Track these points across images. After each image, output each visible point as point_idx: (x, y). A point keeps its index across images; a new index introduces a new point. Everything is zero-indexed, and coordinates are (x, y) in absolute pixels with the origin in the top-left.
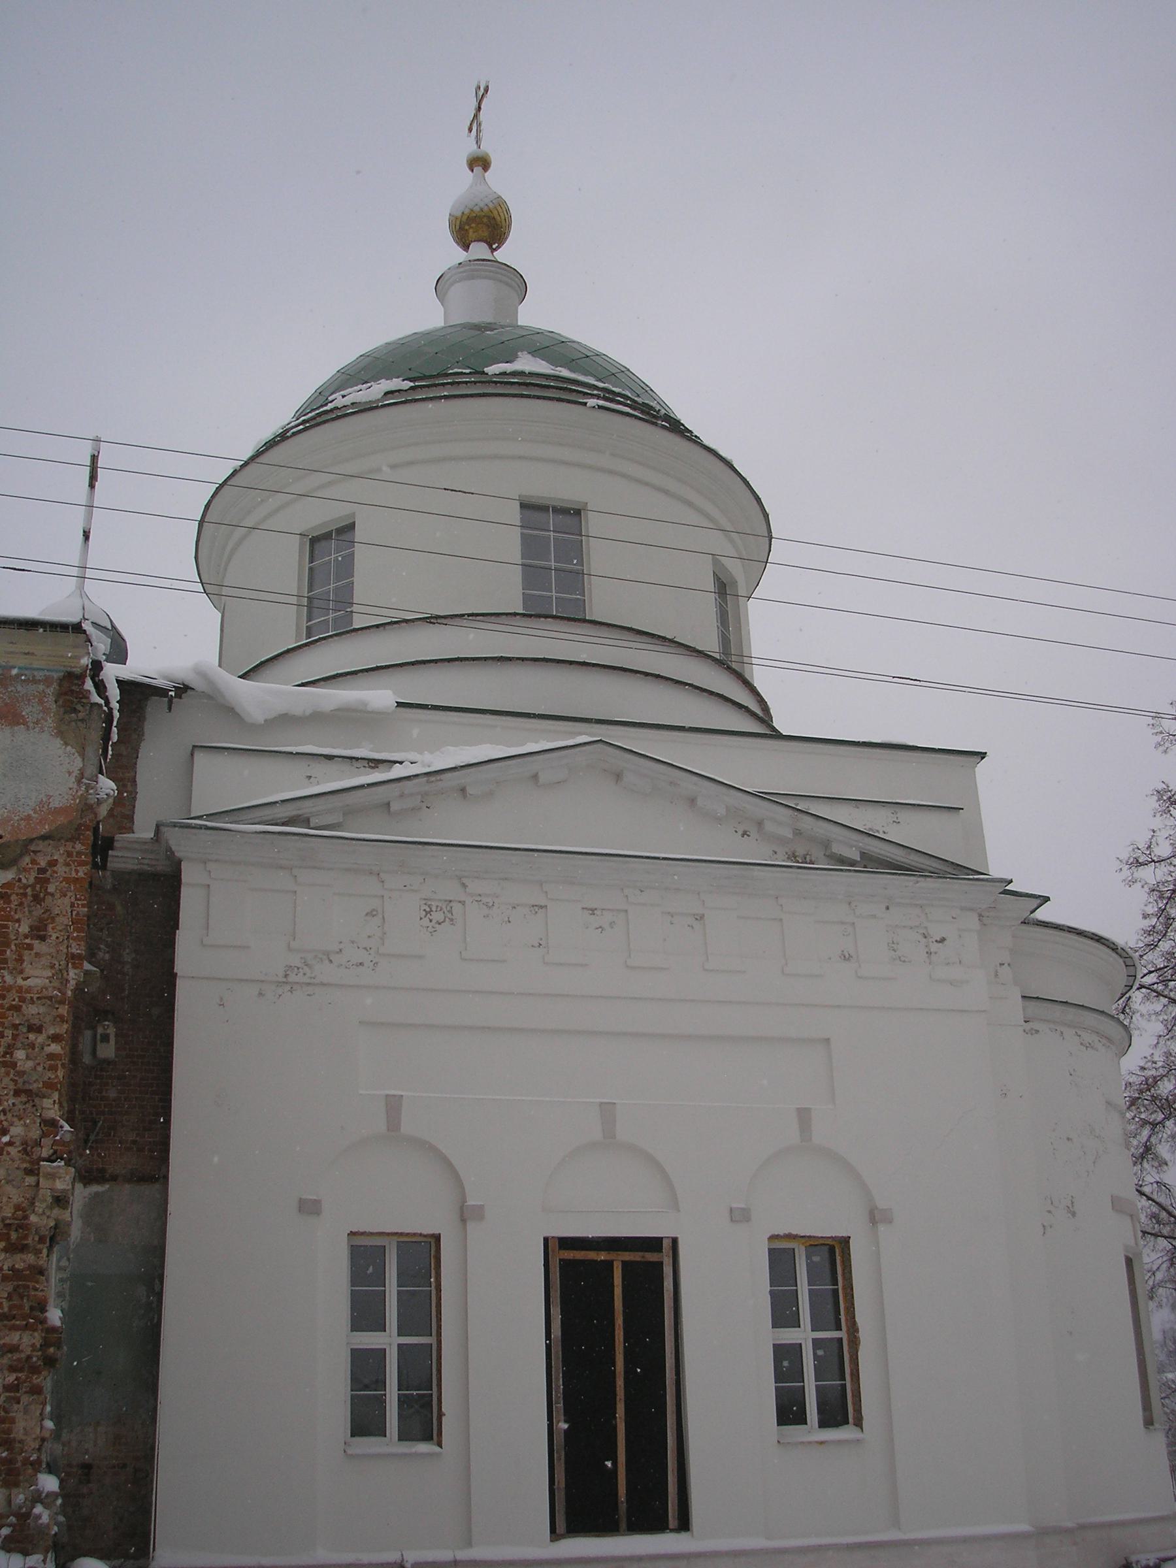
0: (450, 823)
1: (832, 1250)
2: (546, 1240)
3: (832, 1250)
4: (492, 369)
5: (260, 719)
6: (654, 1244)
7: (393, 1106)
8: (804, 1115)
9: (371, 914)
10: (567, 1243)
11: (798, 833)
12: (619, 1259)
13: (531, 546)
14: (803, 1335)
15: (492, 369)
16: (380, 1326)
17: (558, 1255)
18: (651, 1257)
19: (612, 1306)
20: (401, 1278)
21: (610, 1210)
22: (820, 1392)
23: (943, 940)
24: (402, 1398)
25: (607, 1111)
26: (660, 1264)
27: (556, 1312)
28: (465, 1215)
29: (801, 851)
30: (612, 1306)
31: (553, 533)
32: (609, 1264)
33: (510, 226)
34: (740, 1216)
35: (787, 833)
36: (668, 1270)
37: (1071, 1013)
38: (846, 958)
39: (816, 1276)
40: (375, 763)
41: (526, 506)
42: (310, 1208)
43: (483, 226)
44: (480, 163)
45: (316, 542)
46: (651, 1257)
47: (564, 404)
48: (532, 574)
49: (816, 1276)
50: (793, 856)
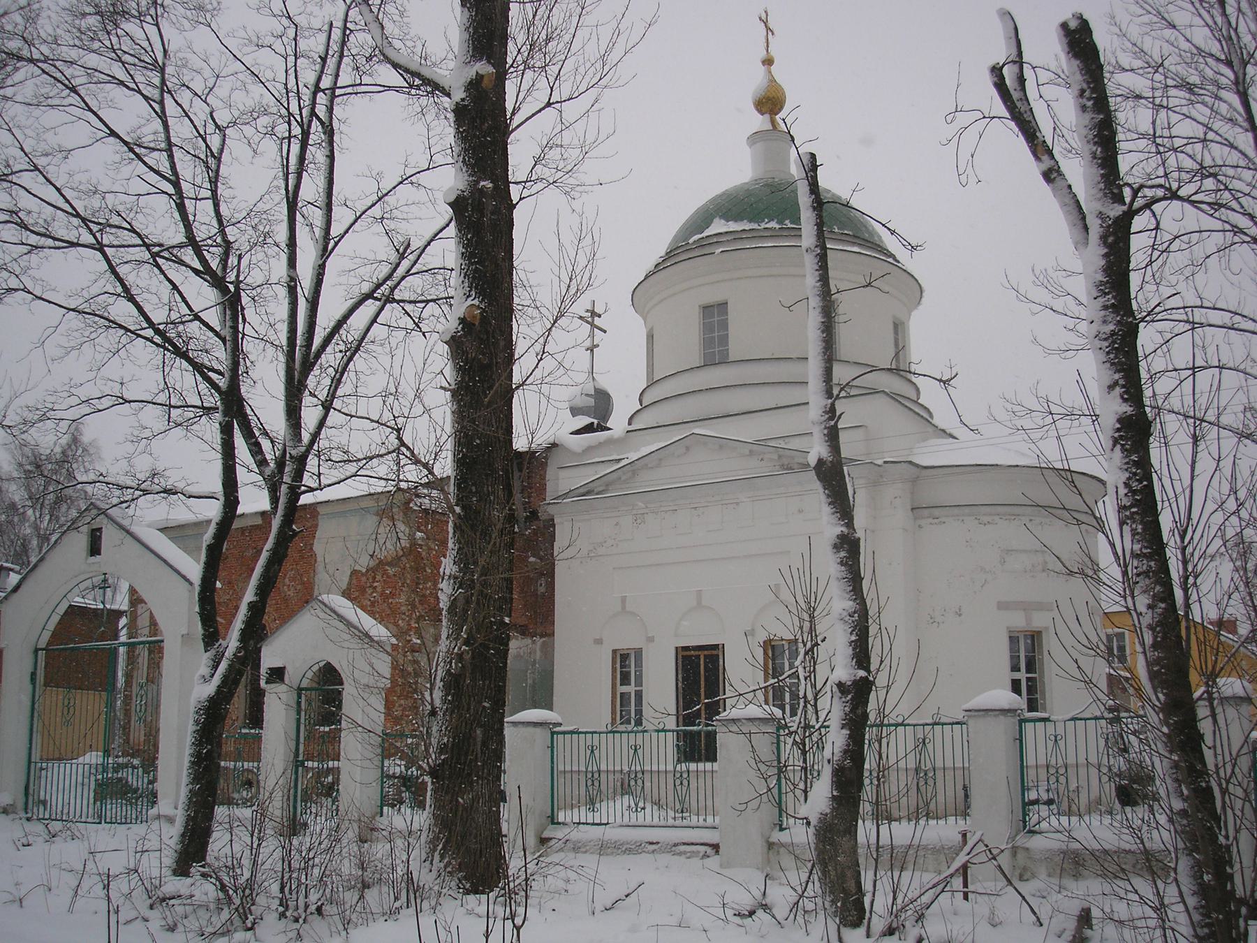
1: (1033, 637)
3: (1033, 637)
4: (691, 241)
5: (579, 450)
6: (715, 647)
7: (624, 600)
9: (617, 524)
10: (685, 648)
11: (780, 457)
12: (702, 654)
14: (1022, 675)
15: (691, 241)
18: (715, 652)
19: (700, 672)
20: (625, 665)
24: (627, 710)
28: (651, 639)
30: (700, 672)
33: (784, 93)
37: (967, 510)
38: (800, 511)
40: (620, 460)
43: (770, 103)
44: (768, 62)
45: (707, 309)
46: (715, 652)
47: (184, 572)
50: (783, 467)
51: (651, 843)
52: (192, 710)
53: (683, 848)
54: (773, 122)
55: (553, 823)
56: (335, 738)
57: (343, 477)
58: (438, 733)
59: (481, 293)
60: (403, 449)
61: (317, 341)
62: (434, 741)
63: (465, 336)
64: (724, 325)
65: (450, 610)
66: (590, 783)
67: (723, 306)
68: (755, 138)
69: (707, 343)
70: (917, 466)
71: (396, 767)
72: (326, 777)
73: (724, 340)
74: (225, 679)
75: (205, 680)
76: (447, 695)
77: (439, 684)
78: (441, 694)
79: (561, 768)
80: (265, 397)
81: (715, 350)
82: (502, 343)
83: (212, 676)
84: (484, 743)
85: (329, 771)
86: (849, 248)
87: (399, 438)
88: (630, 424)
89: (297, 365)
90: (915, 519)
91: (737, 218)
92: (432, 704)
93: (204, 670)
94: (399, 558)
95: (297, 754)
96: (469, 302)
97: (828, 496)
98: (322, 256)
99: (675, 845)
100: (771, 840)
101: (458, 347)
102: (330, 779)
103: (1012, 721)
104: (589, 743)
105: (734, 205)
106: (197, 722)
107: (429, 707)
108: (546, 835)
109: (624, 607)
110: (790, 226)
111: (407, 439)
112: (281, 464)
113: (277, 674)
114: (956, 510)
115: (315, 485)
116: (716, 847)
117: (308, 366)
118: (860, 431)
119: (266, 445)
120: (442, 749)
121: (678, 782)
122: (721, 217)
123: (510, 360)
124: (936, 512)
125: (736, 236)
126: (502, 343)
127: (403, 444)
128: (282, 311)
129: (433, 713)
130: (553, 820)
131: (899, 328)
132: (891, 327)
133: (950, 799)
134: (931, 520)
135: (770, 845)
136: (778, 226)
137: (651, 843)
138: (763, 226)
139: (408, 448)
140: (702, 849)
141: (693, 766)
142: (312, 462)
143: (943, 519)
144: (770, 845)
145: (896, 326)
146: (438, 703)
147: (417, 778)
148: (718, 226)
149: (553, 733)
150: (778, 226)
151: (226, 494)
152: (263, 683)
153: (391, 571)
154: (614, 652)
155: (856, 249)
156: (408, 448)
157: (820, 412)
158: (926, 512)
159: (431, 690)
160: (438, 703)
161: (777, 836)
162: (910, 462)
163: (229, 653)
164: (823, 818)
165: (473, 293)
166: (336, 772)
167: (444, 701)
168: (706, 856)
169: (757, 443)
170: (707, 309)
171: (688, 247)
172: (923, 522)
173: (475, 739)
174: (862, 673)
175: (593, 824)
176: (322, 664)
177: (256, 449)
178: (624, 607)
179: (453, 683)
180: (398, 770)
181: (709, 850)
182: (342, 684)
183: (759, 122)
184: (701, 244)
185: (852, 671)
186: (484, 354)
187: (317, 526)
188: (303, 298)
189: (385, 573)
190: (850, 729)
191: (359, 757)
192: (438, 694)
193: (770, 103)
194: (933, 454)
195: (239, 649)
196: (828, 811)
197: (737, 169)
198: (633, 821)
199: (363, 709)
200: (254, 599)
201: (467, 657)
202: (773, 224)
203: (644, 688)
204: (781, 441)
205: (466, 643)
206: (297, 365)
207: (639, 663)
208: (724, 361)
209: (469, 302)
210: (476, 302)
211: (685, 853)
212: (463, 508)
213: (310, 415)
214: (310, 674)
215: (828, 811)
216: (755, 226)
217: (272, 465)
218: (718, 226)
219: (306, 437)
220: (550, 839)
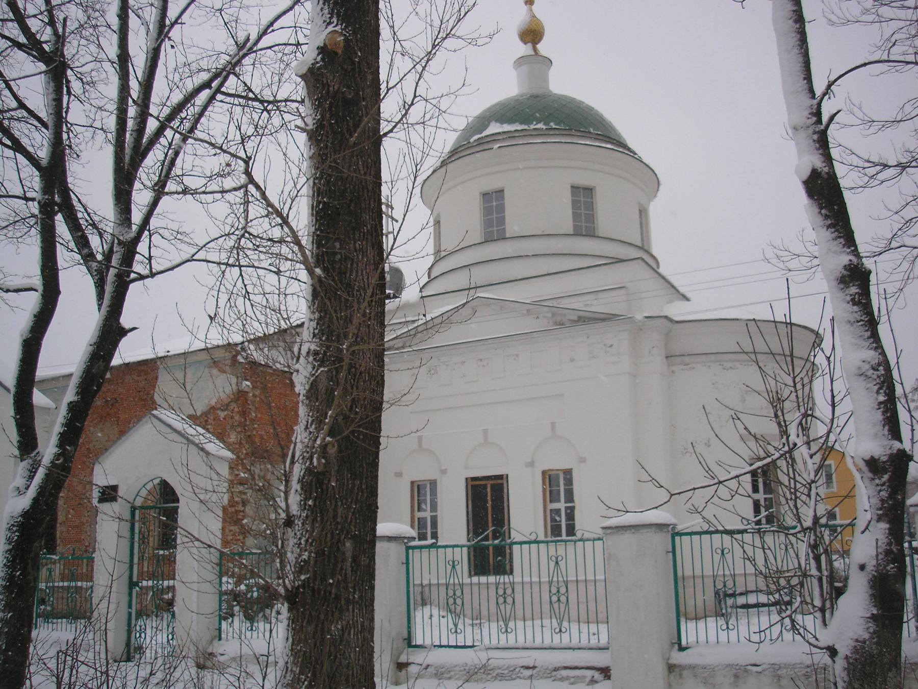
0: (440, 339)
2: (467, 479)
4: (472, 140)
6: (500, 477)
8: (553, 425)
10: (473, 479)
11: (553, 314)
12: (489, 483)
13: (575, 204)
14: (761, 496)
15: (472, 140)
16: (559, 501)
17: (470, 483)
18: (500, 481)
19: (487, 500)
20: (423, 493)
21: (485, 466)
22: (561, 526)
23: (611, 346)
24: (427, 529)
25: (485, 431)
26: (502, 484)
27: (470, 502)
28: (444, 472)
29: (558, 320)
30: (487, 500)
31: (583, 197)
32: (485, 486)
34: (531, 464)
35: (550, 315)
36: (505, 486)
37: (713, 357)
38: (572, 360)
39: (557, 485)
40: (414, 321)
41: (572, 187)
42: (399, 475)
43: (532, 34)
45: (486, 196)
46: (500, 481)
48: (576, 216)
49: (557, 485)
50: (556, 323)
51: (528, 668)
52: (5, 526)
53: (565, 673)
54: (535, 49)
55: (410, 645)
56: (171, 561)
57: (178, 260)
58: (294, 547)
59: (344, 19)
60: (251, 188)
61: (152, 125)
62: (291, 557)
63: (325, 66)
64: (501, 209)
65: (308, 396)
66: (501, 600)
67: (500, 192)
68: (520, 62)
69: (488, 224)
70: (671, 320)
71: (228, 584)
72: (168, 593)
73: (502, 221)
74: (42, 491)
75: (20, 492)
76: (306, 499)
77: (295, 485)
78: (298, 498)
79: (417, 582)
80: (91, 178)
81: (494, 226)
82: (370, 77)
83: (27, 488)
84: (355, 559)
85: (164, 591)
86: (604, 145)
87: (248, 173)
88: (421, 291)
89: (128, 150)
90: (669, 365)
91: (511, 121)
92: (287, 511)
93: (20, 482)
94: (227, 405)
95: (131, 577)
96: (330, 28)
97: (826, 217)
98: (157, 40)
99: (556, 669)
100: (672, 661)
101: (317, 80)
102: (170, 595)
103: (661, 541)
104: (449, 557)
105: (506, 112)
106: (9, 540)
107: (283, 515)
108: (403, 659)
109: (420, 445)
110: (554, 126)
111: (257, 176)
112: (108, 256)
113: (109, 494)
114: (704, 358)
115: (146, 272)
116: (606, 672)
117: (140, 153)
118: (622, 291)
119: (95, 241)
120: (301, 568)
121: (555, 598)
122: (497, 121)
123: (376, 99)
124: (687, 359)
125: (510, 135)
126: (370, 77)
127: (251, 181)
128: (112, 90)
129: (289, 522)
130: (409, 642)
131: (643, 213)
132: (638, 212)
133: (700, 602)
134: (683, 367)
135: (671, 668)
136: (544, 127)
137: (528, 668)
138: (532, 127)
139: (258, 187)
140: (589, 673)
141: (483, 579)
142: (142, 247)
143: (692, 365)
144: (671, 668)
145: (640, 212)
146: (295, 509)
147: (246, 594)
148: (494, 128)
149: (408, 548)
150: (544, 127)
151: (45, 285)
152: (95, 501)
153: (222, 415)
154: (412, 483)
155: (609, 146)
156: (258, 187)
157: (806, 113)
158: (678, 360)
159: (286, 493)
160: (295, 509)
161: (678, 658)
162: (666, 317)
163: (46, 460)
164: (860, 647)
165: (335, 20)
166: (172, 589)
167: (303, 506)
168: (593, 681)
169: (534, 303)
170: (486, 196)
171: (471, 144)
172: (675, 368)
173: (344, 553)
174: (897, 445)
175: (456, 647)
176: (157, 481)
177: (82, 242)
178: (420, 445)
179: (314, 483)
180: (230, 587)
181: (597, 675)
182: (178, 501)
183: (524, 49)
184: (480, 142)
185: (886, 442)
186: (348, 87)
187: (157, 378)
188: (133, 100)
189: (216, 418)
190: (889, 522)
191: (195, 578)
192: (295, 500)
193: (532, 34)
194: (678, 310)
195: (57, 456)
196: (866, 636)
197: (506, 86)
198: (503, 643)
199: (199, 522)
200: (76, 399)
201: (332, 451)
202: (541, 126)
203: (439, 513)
204: (554, 301)
205: (331, 433)
206: (128, 150)
207: (434, 492)
208: (502, 237)
209: (330, 28)
210: (338, 28)
211: (568, 678)
212: (324, 269)
213: (141, 197)
214: (144, 493)
215: (866, 636)
216: (526, 127)
217: (99, 257)
218: (494, 128)
219: (137, 217)
220: (407, 664)
